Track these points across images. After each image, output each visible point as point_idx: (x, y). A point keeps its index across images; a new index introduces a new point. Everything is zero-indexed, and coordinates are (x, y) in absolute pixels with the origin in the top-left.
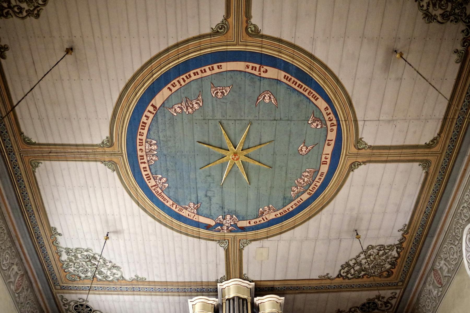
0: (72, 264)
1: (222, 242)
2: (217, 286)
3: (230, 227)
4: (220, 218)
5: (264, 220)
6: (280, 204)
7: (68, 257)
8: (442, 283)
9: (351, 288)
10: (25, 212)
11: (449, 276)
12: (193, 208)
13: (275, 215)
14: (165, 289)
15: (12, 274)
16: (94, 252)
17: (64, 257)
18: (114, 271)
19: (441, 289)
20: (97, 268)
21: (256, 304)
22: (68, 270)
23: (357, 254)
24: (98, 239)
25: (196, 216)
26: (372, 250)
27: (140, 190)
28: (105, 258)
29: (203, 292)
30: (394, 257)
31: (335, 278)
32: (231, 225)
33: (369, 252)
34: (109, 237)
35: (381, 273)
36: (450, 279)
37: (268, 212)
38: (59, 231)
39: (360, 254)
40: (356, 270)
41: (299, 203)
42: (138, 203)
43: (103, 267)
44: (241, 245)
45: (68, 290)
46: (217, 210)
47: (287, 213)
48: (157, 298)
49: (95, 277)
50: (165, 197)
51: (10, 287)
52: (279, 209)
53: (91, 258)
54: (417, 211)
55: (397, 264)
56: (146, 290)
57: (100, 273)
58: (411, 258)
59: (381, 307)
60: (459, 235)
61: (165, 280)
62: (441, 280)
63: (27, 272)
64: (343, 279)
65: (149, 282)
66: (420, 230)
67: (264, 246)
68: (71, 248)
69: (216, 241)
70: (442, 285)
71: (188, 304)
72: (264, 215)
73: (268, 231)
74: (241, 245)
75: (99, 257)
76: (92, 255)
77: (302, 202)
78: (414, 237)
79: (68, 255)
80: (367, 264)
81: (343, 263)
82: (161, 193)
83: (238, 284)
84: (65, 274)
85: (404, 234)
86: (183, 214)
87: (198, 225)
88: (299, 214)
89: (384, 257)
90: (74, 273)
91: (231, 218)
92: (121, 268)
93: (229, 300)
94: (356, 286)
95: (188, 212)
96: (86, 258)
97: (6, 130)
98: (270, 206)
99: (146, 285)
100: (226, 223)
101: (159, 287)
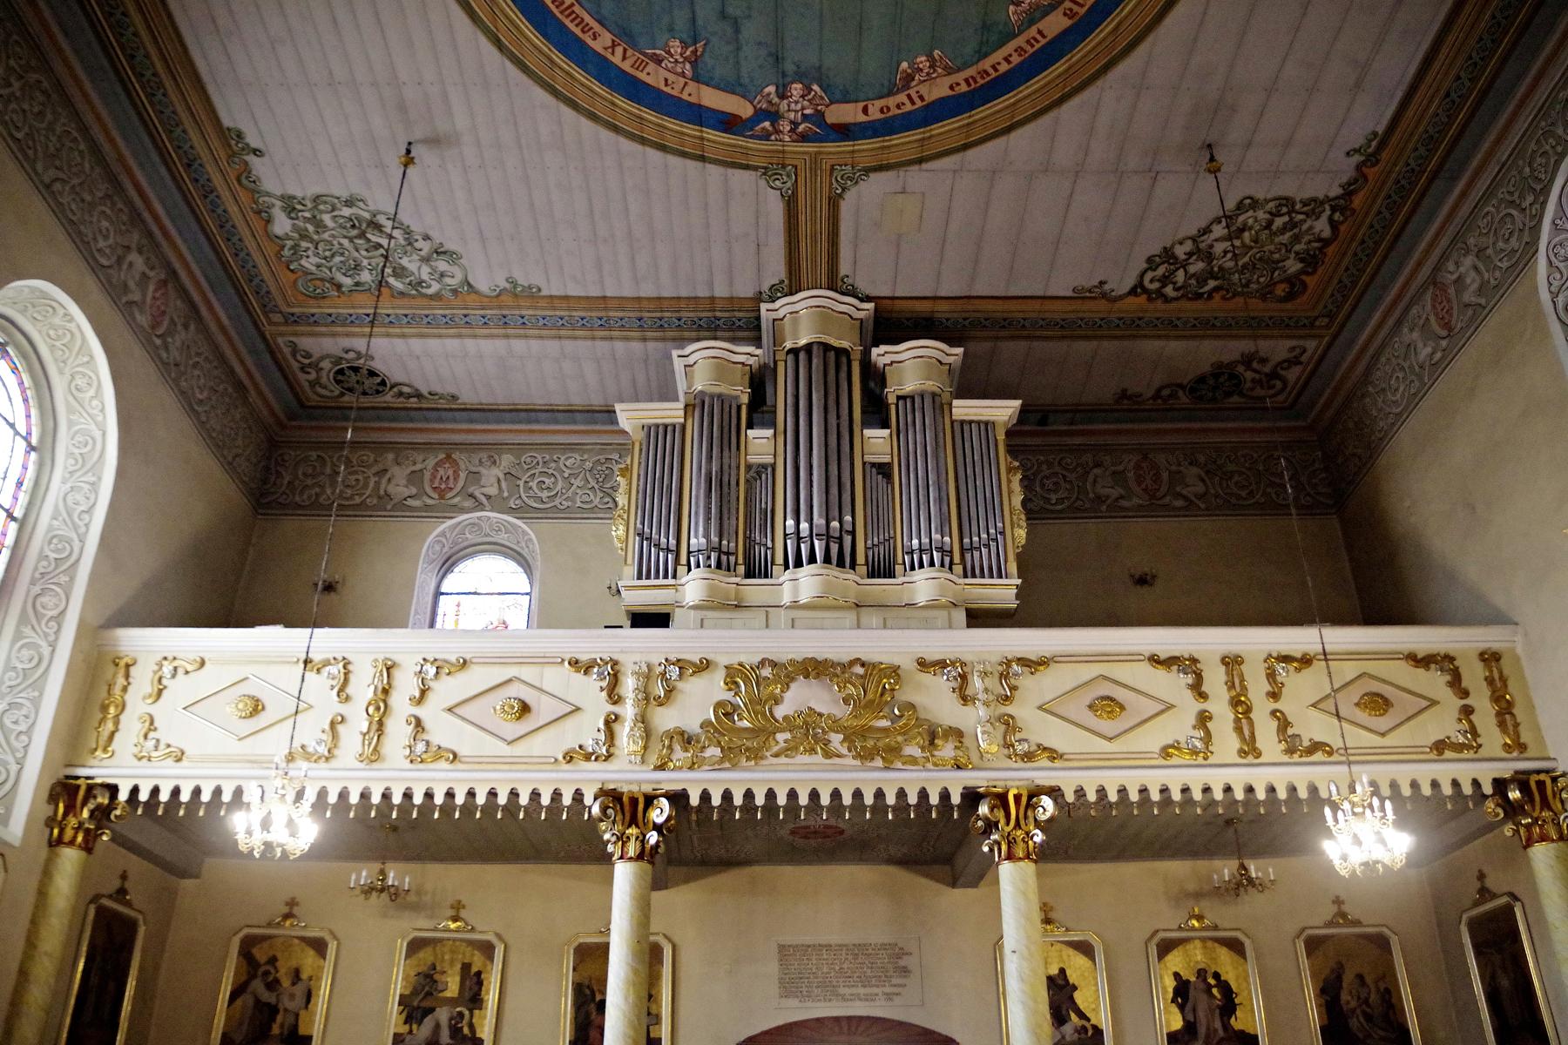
0: (310, 245)
1: (776, 174)
2: (759, 310)
3: (800, 124)
4: (769, 94)
5: (913, 103)
6: (969, 49)
7: (294, 225)
8: (1453, 322)
9: (1170, 327)
10: (133, 79)
11: (1480, 305)
12: (681, 60)
13: (951, 88)
14: (600, 319)
15: (133, 277)
16: (372, 207)
17: (282, 225)
18: (442, 265)
19: (1444, 343)
20: (386, 257)
21: (875, 365)
22: (300, 265)
23: (1203, 224)
24: (381, 165)
25: (692, 86)
26: (1250, 213)
28: (408, 227)
29: (717, 328)
30: (1320, 240)
31: (1121, 297)
32: (805, 118)
33: (1241, 218)
34: (413, 158)
35: (1267, 286)
36: (1478, 314)
37: (928, 74)
38: (253, 140)
39: (1211, 224)
40: (1194, 275)
41: (1032, 46)
42: (499, 40)
43: (405, 253)
44: (835, 185)
45: (309, 324)
46: (760, 67)
47: (989, 78)
48: (582, 347)
49: (384, 284)
50: (588, 19)
51: (134, 319)
52: (965, 66)
53: (364, 226)
54: (1423, 88)
55: (1323, 262)
56: (541, 322)
57: (400, 272)
58: (1371, 245)
59: (1252, 389)
60: (1543, 177)
61: (598, 294)
62: (1451, 315)
63: (174, 273)
64: (1150, 299)
65: (551, 297)
66: (1417, 153)
67: (908, 190)
68: (299, 194)
69: (756, 168)
70: (1450, 330)
71: (672, 364)
72: (914, 83)
73: (923, 139)
74: (835, 185)
75: (389, 224)
76: (367, 215)
77: (1043, 41)
78: (1394, 175)
79: (292, 219)
80: (1229, 255)
81: (1156, 249)
82: (573, 5)
83: (824, 307)
84: (292, 277)
85: (1364, 163)
86: (648, 80)
87: (698, 115)
88: (1029, 84)
89: (1285, 238)
90: (320, 275)
91: (806, 92)
92: (461, 258)
93: (794, 352)
94: (1186, 323)
95: (663, 74)
96: (348, 225)
97: (162, 90)
98: (937, 53)
99: (543, 308)
100: (789, 110)
101: (582, 314)
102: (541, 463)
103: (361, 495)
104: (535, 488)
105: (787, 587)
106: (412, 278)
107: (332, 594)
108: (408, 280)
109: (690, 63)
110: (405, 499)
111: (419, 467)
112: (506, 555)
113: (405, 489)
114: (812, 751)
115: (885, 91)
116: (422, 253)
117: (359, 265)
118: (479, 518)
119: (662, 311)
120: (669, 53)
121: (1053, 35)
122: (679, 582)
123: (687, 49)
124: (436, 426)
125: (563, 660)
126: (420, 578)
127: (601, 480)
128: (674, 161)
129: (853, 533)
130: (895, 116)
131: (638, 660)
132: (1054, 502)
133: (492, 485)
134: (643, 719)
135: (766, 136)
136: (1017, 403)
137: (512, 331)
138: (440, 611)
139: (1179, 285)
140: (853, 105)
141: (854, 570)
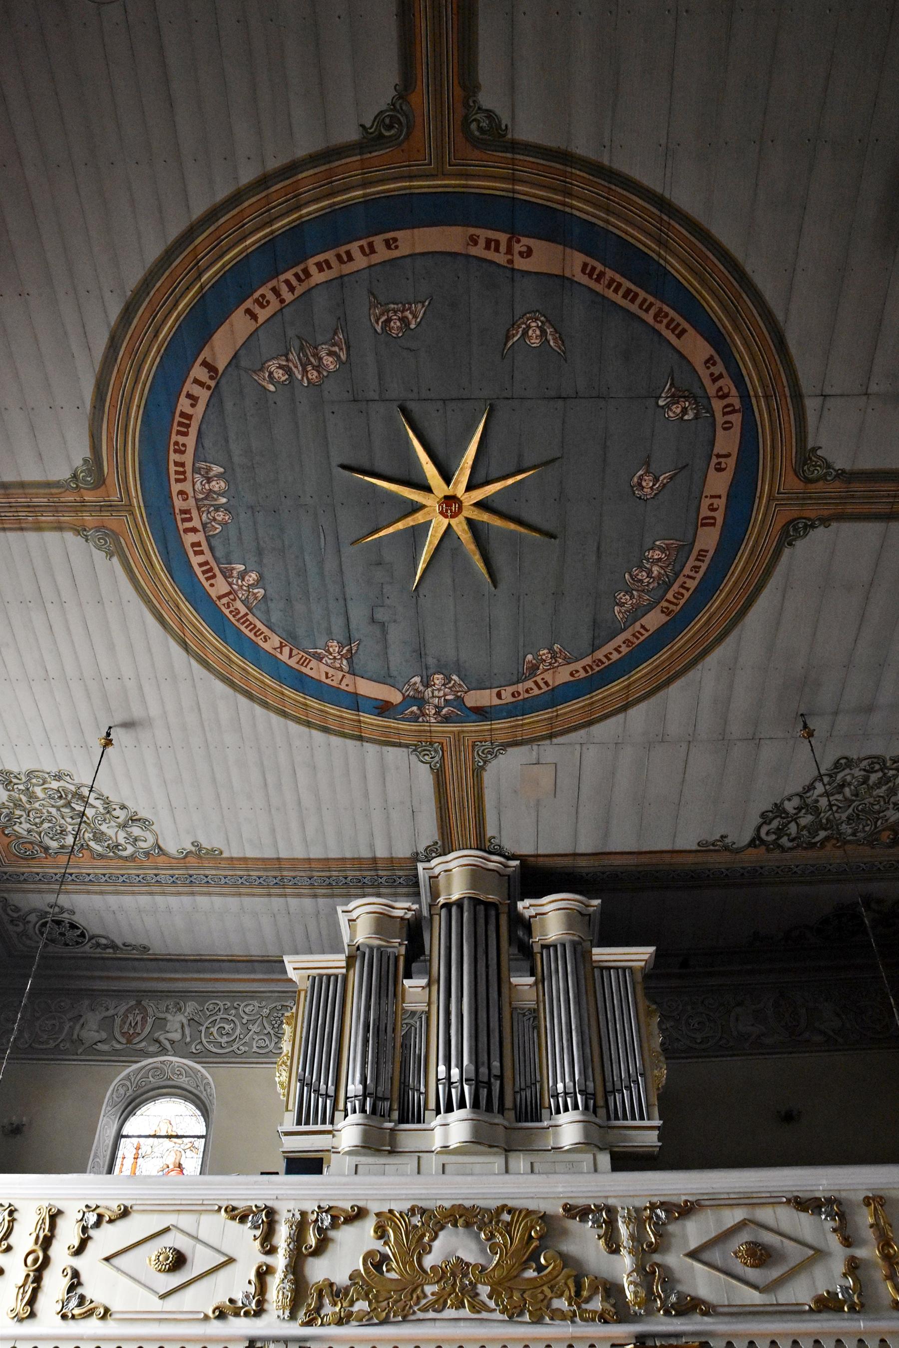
0: (22, 813)
1: (425, 750)
3: (443, 708)
4: (415, 684)
5: (540, 688)
7: (10, 796)
14: (275, 878)
18: (136, 831)
25: (349, 679)
26: (847, 771)
27: (186, 608)
29: (379, 886)
37: (550, 664)
40: (805, 827)
41: (638, 638)
47: (603, 666)
50: (259, 625)
53: (70, 796)
56: (223, 881)
57: (99, 837)
64: (768, 850)
65: (232, 859)
68: (15, 770)
69: (407, 746)
72: (539, 672)
76: (73, 788)
77: (647, 634)
79: (9, 790)
82: (247, 614)
86: (311, 673)
87: (355, 702)
89: (882, 791)
92: (153, 824)
93: (447, 906)
99: (224, 869)
100: (433, 697)
102: (222, 1009)
103: (55, 1039)
104: (215, 1033)
105: (438, 1131)
106: (110, 842)
107: (18, 1136)
108: (106, 844)
109: (346, 659)
110: (95, 1044)
111: (111, 1012)
112: (186, 1099)
113: (96, 1034)
114: (460, 1305)
115: (515, 679)
116: (119, 820)
117: (65, 831)
118: (162, 1062)
119: (330, 871)
120: (328, 651)
121: (655, 628)
122: (336, 1128)
123: (343, 648)
124: (132, 975)
125: (220, 1208)
126: (103, 1120)
127: (276, 1025)
128: (335, 740)
129: (501, 1077)
130: (524, 699)
131: (291, 1208)
132: (699, 1041)
133: (176, 1031)
134: (296, 1268)
135: (415, 719)
136: (651, 949)
137: (197, 889)
138: (120, 1154)
139: (794, 835)
140: (488, 691)
141: (503, 1115)
